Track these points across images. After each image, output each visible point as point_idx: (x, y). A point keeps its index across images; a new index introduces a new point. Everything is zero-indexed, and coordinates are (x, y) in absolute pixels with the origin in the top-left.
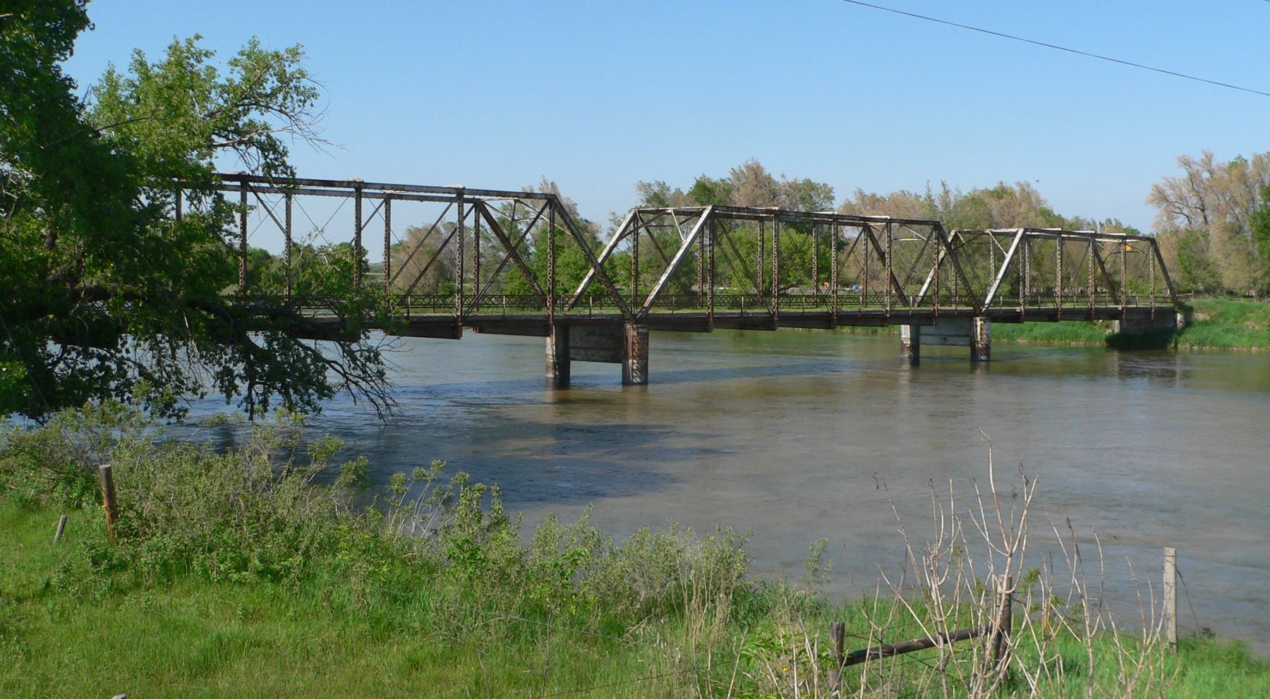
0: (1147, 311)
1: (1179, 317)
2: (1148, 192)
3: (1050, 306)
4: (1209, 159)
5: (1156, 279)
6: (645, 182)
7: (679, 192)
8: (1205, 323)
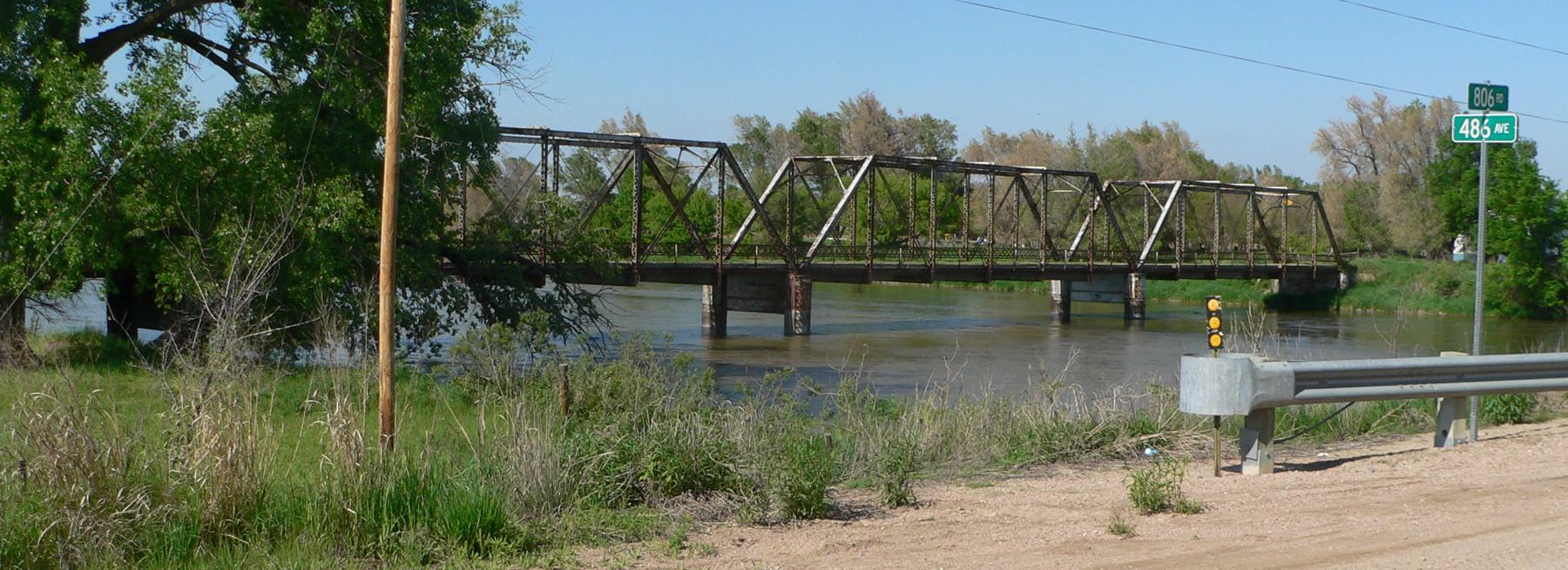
0: (1309, 270)
1: (1342, 277)
2: (1312, 138)
3: (1207, 263)
4: (1382, 100)
5: (1319, 235)
6: (744, 116)
7: (780, 129)
8: (1370, 284)
